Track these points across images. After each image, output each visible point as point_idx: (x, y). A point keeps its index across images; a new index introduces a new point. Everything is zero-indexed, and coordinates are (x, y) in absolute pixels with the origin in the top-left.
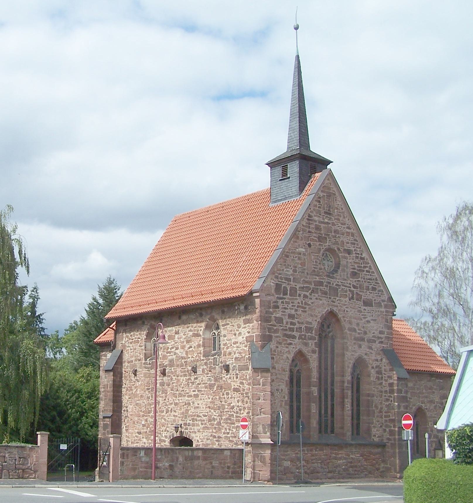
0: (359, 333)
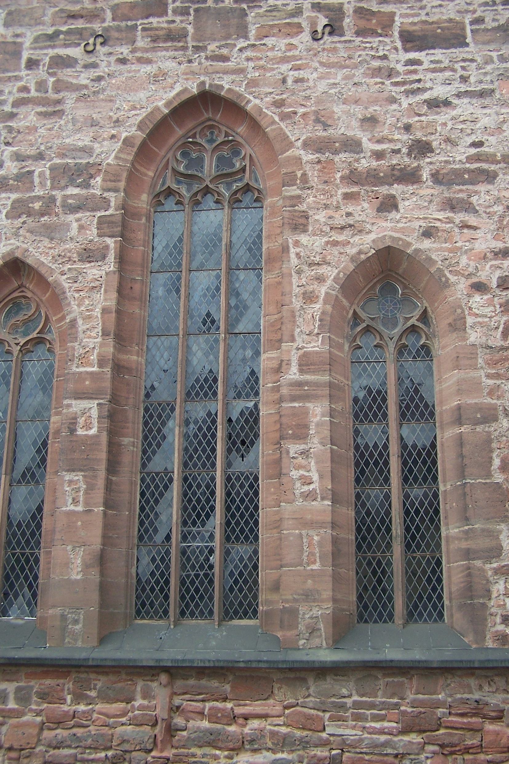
0: (379, 155)
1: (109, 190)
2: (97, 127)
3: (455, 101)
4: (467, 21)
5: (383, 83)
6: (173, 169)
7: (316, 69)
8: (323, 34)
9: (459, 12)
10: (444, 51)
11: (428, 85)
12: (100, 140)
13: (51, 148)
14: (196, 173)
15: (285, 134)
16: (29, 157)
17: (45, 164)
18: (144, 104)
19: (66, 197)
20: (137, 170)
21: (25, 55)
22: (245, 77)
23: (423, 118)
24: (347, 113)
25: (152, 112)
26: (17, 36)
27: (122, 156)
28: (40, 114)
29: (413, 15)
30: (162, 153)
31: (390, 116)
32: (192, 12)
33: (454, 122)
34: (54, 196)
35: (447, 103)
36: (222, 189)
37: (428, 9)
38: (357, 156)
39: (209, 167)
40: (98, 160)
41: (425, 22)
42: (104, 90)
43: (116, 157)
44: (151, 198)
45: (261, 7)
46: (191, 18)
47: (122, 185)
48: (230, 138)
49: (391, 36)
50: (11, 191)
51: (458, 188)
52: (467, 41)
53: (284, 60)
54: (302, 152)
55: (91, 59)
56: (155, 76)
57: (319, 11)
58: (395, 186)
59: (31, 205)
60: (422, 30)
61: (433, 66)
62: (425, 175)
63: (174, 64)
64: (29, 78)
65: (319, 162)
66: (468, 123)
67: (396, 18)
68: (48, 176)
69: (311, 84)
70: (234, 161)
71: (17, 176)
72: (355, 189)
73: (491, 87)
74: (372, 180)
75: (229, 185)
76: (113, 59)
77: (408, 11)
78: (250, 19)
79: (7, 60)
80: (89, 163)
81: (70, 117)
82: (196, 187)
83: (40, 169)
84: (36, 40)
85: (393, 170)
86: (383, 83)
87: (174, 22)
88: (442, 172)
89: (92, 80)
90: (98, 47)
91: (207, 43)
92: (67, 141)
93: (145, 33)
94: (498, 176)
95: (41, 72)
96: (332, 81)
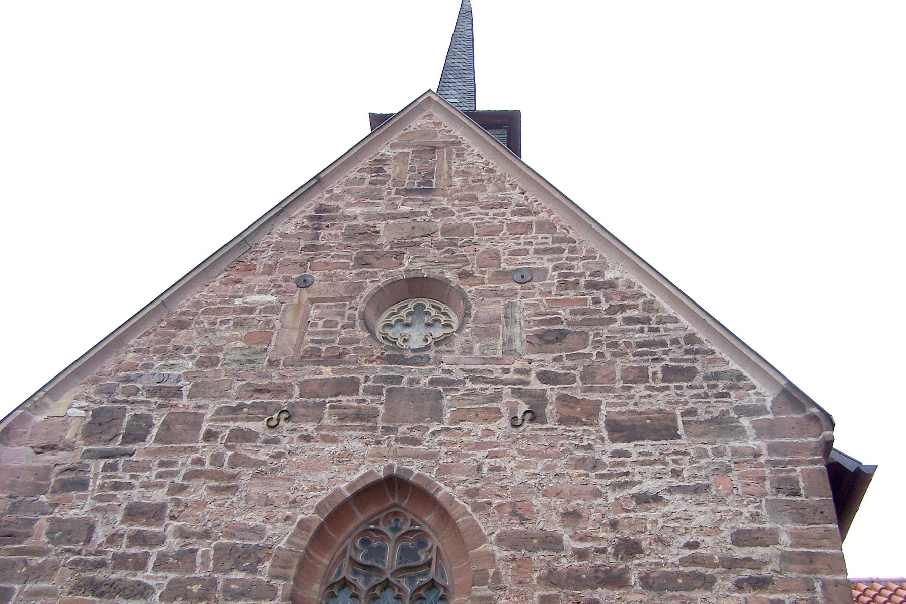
0: (581, 554)
1: (277, 577)
2: (272, 507)
3: (667, 497)
4: (678, 413)
5: (587, 475)
6: (351, 558)
7: (514, 458)
8: (524, 420)
9: (669, 402)
10: (654, 443)
11: (637, 478)
12: (273, 520)
13: (219, 525)
14: (376, 564)
15: (477, 526)
16: (194, 534)
17: (210, 543)
18: (325, 485)
19: (229, 581)
20: (311, 557)
21: (205, 427)
22: (437, 462)
23: (631, 515)
24: (548, 507)
25: (332, 495)
26: (200, 407)
27: (296, 540)
28: (211, 488)
29: (621, 405)
30: (340, 539)
31: (595, 512)
32: (384, 392)
33: (665, 519)
34: (216, 579)
35: (657, 499)
36: (404, 584)
37: (636, 399)
38: (556, 555)
39: (391, 559)
40: (269, 543)
41: (633, 412)
42: (283, 467)
43: (289, 541)
44: (323, 588)
45: (458, 390)
46: (383, 398)
47: (292, 572)
48: (417, 527)
49: (597, 425)
50: (169, 570)
51: (670, 594)
52: (679, 433)
53: (480, 446)
54: (495, 548)
55: (273, 435)
56: (340, 456)
57: (520, 397)
58: (600, 589)
59: (188, 587)
60: (630, 420)
61: (641, 458)
62: (633, 578)
63: (361, 445)
64: (205, 450)
65: (514, 559)
66: (682, 521)
67: (602, 407)
68: (212, 557)
69: (508, 473)
70: (419, 553)
71: (178, 554)
72: (554, 592)
73: (706, 482)
74: (574, 582)
75: (412, 580)
76: (296, 436)
77: (615, 400)
78: (445, 401)
79: (185, 431)
80: (258, 545)
81: (244, 494)
82: (375, 580)
83: (205, 548)
84: (218, 412)
85: (597, 571)
86: (587, 475)
87: (364, 400)
88: (652, 576)
89: (272, 457)
90: (282, 422)
91: (398, 424)
92: (238, 519)
93: (333, 411)
94: (716, 581)
95: (219, 445)
96: (531, 471)
